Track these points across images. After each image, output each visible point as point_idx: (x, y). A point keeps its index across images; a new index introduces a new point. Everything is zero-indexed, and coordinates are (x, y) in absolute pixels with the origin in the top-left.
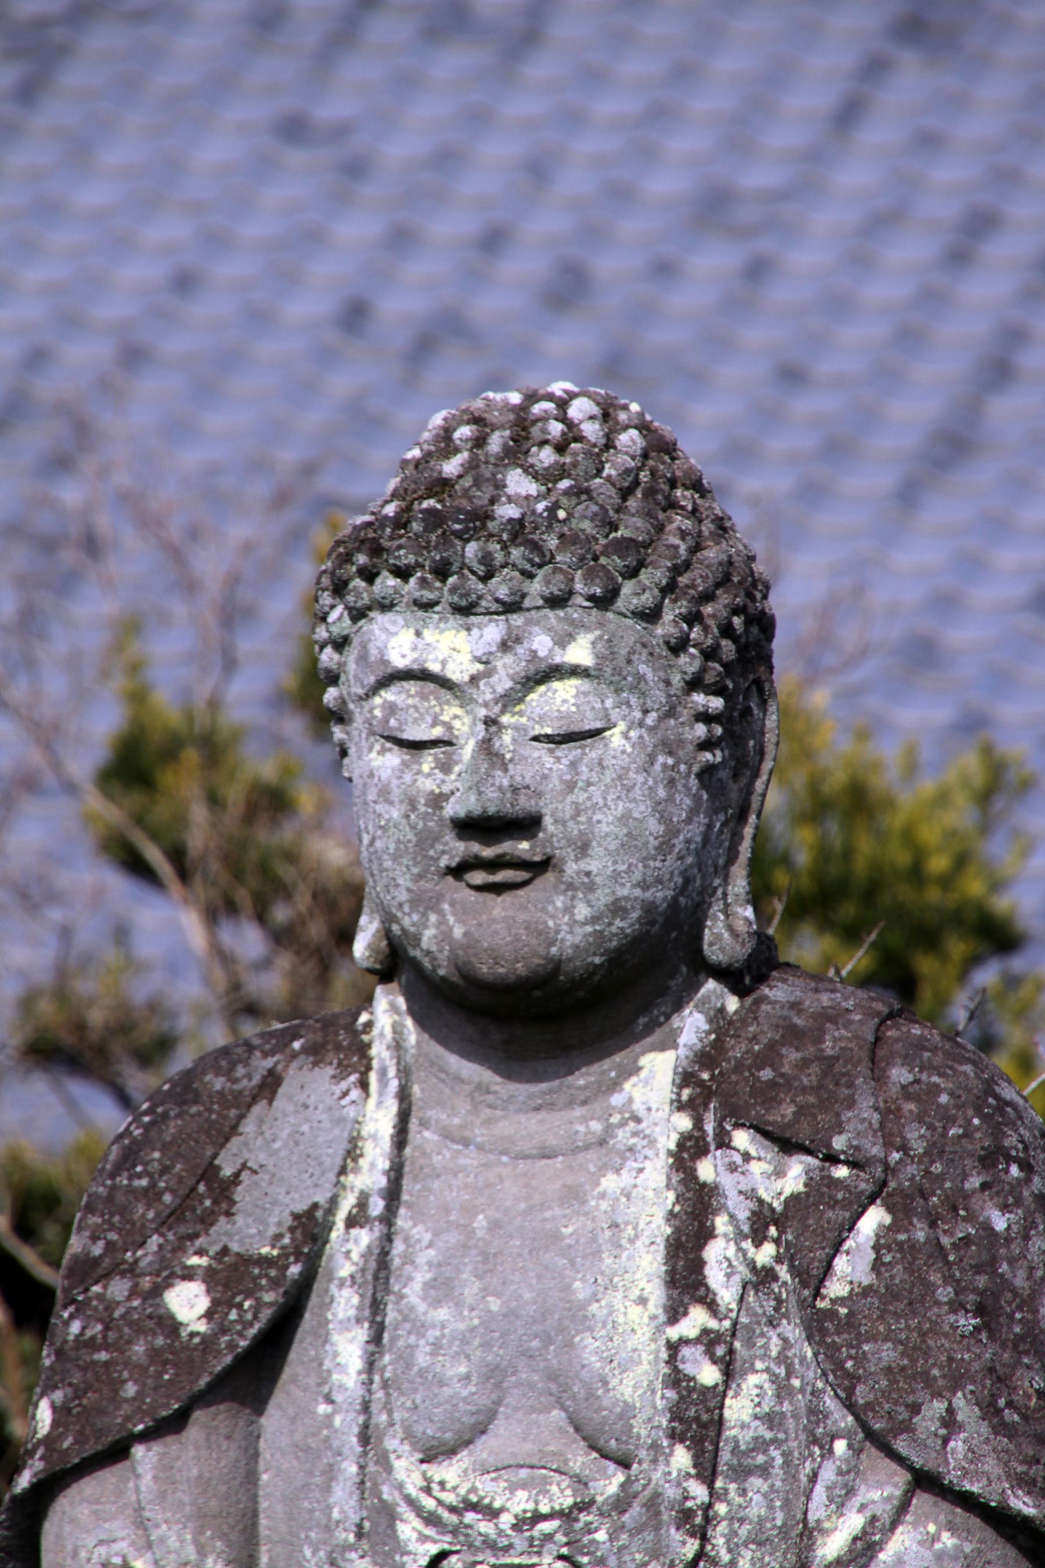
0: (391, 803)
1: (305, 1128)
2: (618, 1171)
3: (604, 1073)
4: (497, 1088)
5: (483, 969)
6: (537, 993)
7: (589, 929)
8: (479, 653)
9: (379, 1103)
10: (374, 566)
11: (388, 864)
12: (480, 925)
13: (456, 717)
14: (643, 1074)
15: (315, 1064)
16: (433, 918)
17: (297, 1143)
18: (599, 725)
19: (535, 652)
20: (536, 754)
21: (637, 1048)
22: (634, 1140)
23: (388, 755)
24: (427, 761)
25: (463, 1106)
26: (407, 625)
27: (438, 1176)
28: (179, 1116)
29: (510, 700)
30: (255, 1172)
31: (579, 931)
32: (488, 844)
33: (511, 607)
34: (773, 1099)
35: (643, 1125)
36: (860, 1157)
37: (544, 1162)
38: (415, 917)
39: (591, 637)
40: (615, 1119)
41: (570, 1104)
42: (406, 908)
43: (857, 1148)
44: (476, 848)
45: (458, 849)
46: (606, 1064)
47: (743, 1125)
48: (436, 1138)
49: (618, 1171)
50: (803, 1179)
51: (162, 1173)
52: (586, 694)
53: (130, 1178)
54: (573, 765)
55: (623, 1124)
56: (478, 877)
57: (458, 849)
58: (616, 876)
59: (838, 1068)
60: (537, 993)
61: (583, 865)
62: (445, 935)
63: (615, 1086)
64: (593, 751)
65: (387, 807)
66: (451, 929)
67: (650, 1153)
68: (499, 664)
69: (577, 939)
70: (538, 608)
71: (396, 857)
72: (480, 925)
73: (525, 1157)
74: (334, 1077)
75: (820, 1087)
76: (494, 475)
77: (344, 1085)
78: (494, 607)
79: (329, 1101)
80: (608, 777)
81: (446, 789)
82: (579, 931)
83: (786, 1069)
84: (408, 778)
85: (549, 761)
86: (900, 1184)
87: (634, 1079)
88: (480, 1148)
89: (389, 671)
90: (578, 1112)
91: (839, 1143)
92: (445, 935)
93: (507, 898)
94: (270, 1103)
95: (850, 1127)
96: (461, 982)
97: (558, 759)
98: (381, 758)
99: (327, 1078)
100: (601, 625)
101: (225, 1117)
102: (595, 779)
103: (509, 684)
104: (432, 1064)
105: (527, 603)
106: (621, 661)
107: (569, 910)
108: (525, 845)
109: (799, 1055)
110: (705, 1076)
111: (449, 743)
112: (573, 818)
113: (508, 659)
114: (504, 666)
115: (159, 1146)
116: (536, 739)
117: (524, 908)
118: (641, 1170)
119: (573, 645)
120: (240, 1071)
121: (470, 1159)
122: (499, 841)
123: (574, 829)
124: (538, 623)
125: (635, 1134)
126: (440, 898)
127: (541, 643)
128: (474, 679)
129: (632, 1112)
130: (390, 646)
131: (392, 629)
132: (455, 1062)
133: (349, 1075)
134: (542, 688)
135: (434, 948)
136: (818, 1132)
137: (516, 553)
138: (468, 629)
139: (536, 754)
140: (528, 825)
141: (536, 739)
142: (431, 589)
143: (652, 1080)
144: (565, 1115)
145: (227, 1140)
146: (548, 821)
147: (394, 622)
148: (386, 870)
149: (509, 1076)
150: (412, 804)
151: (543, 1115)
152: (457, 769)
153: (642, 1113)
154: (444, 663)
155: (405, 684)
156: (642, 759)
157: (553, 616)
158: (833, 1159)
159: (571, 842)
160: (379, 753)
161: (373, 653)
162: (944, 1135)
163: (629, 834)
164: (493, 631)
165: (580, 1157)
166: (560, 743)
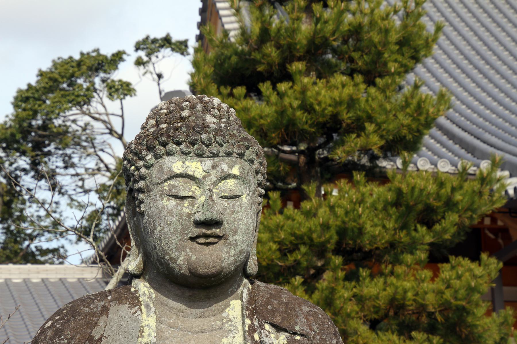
0: (173, 216)
1: (123, 323)
2: (227, 337)
3: (220, 306)
4: (186, 311)
5: (201, 270)
6: (213, 279)
7: (233, 258)
8: (206, 169)
9: (148, 316)
10: (168, 141)
11: (169, 236)
12: (202, 256)
13: (196, 189)
14: (231, 307)
15: (120, 304)
16: (183, 253)
17: (120, 328)
18: (240, 194)
19: (223, 170)
20: (222, 202)
21: (229, 299)
22: (230, 328)
23: (171, 201)
24: (186, 203)
25: (174, 317)
26: (179, 160)
27: (168, 339)
28: (74, 320)
29: (215, 184)
30: (107, 338)
31: (231, 259)
32: (208, 229)
33: (215, 155)
34: (274, 315)
35: (233, 323)
36: (304, 333)
37: (203, 334)
38: (177, 253)
39: (238, 166)
40: (225, 321)
41: (209, 316)
42: (174, 250)
43: (303, 330)
44: (203, 230)
45: (198, 231)
46: (221, 303)
47: (267, 323)
48: (165, 327)
49: (227, 337)
50: (286, 340)
51: (72, 339)
52: (237, 184)
53: (60, 340)
54: (233, 205)
55: (227, 322)
56: (202, 240)
57: (198, 231)
58: (243, 242)
59: (289, 306)
60: (213, 279)
61: (235, 238)
62: (188, 259)
63: (223, 310)
64: (238, 202)
65: (171, 217)
66: (190, 257)
67: (236, 331)
68: (212, 173)
69: (229, 261)
70: (223, 156)
71: (173, 234)
72: (202, 256)
73: (197, 333)
74: (129, 307)
75: (286, 311)
76: (202, 116)
77: (134, 310)
78: (210, 155)
79: (129, 315)
80: (243, 210)
81: (193, 212)
82: (231, 259)
83: (275, 306)
84: (179, 208)
85: (226, 204)
86: (316, 342)
87: (229, 308)
88: (181, 330)
89: (173, 174)
90: (212, 318)
91: (297, 328)
92: (188, 259)
93: (210, 247)
94: (107, 316)
95: (299, 323)
96: (189, 275)
97: (229, 204)
98: (168, 202)
99: (127, 308)
100: (241, 163)
101: (92, 320)
102: (239, 211)
103: (215, 179)
104: (162, 303)
105: (220, 155)
106: (246, 175)
107: (228, 252)
108: (218, 230)
109: (277, 302)
110: (251, 308)
111: (194, 198)
112: (233, 222)
113: (215, 171)
114: (213, 173)
115: (69, 330)
116: (221, 197)
117: (216, 250)
118: (234, 337)
119: (234, 168)
120: (92, 306)
121: (178, 333)
122: (209, 228)
123: (233, 226)
124: (223, 161)
125: (231, 325)
126: (186, 247)
127: (225, 167)
128: (204, 177)
129: (229, 319)
130: (173, 166)
131: (173, 161)
132: (171, 302)
133: (135, 306)
134: (223, 182)
135: (182, 263)
136: (290, 325)
137: (219, 138)
138: (201, 162)
139: (222, 202)
140: (217, 223)
141: (221, 197)
142: (190, 148)
143: (234, 308)
144: (208, 319)
145: (94, 327)
146: (225, 223)
147: (174, 159)
148: (168, 238)
149: (190, 307)
150: (181, 216)
151: (200, 319)
152: (196, 206)
153: (232, 319)
154: (194, 172)
155: (178, 179)
156: (250, 206)
157: (227, 159)
158: (295, 333)
159: (232, 230)
160: (166, 201)
161: (166, 169)
162: (323, 327)
163: (247, 229)
164: (209, 163)
165: (214, 333)
166: (229, 199)
